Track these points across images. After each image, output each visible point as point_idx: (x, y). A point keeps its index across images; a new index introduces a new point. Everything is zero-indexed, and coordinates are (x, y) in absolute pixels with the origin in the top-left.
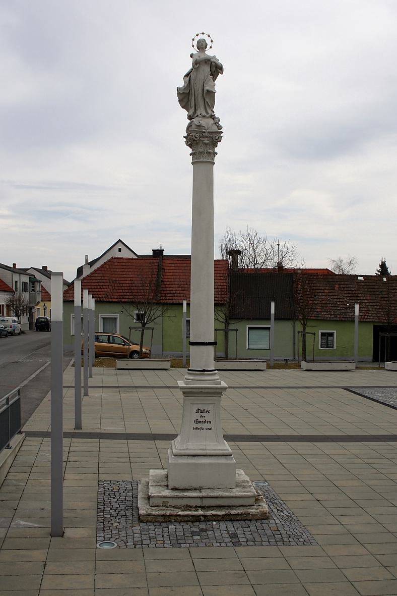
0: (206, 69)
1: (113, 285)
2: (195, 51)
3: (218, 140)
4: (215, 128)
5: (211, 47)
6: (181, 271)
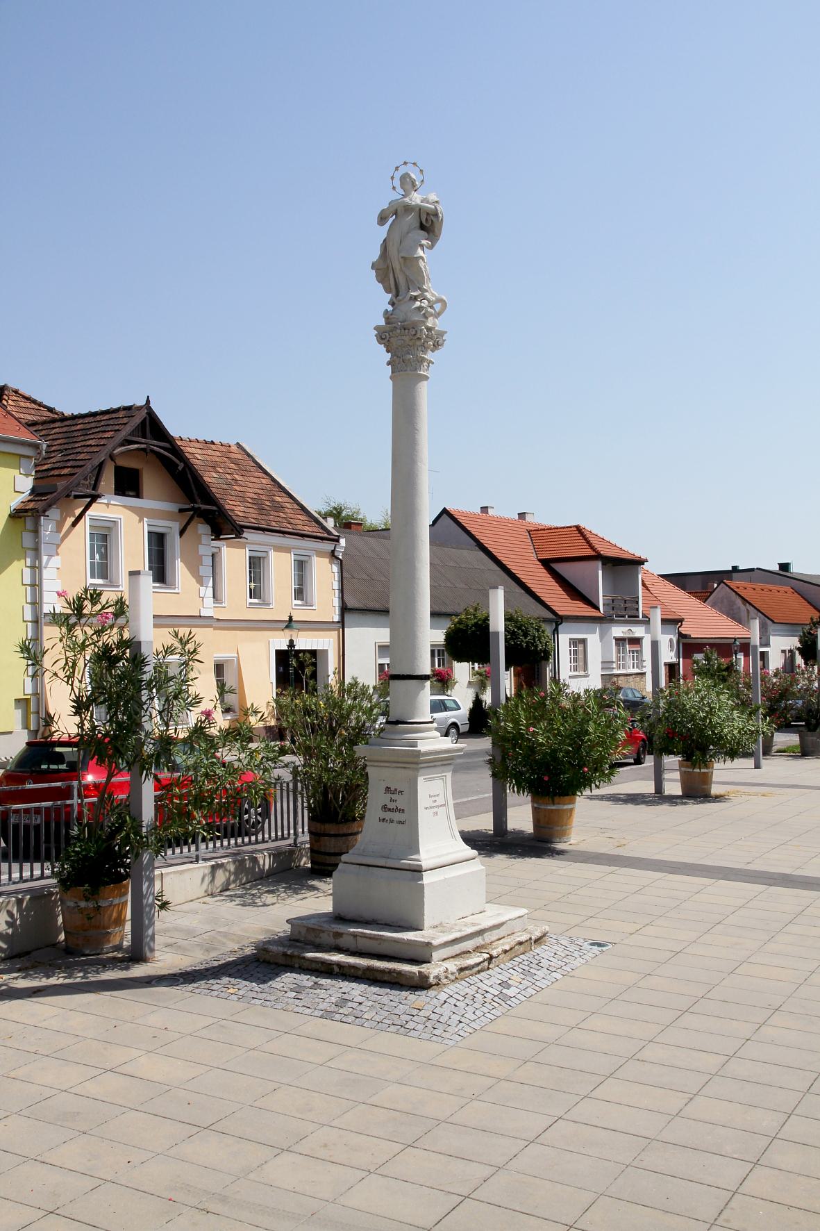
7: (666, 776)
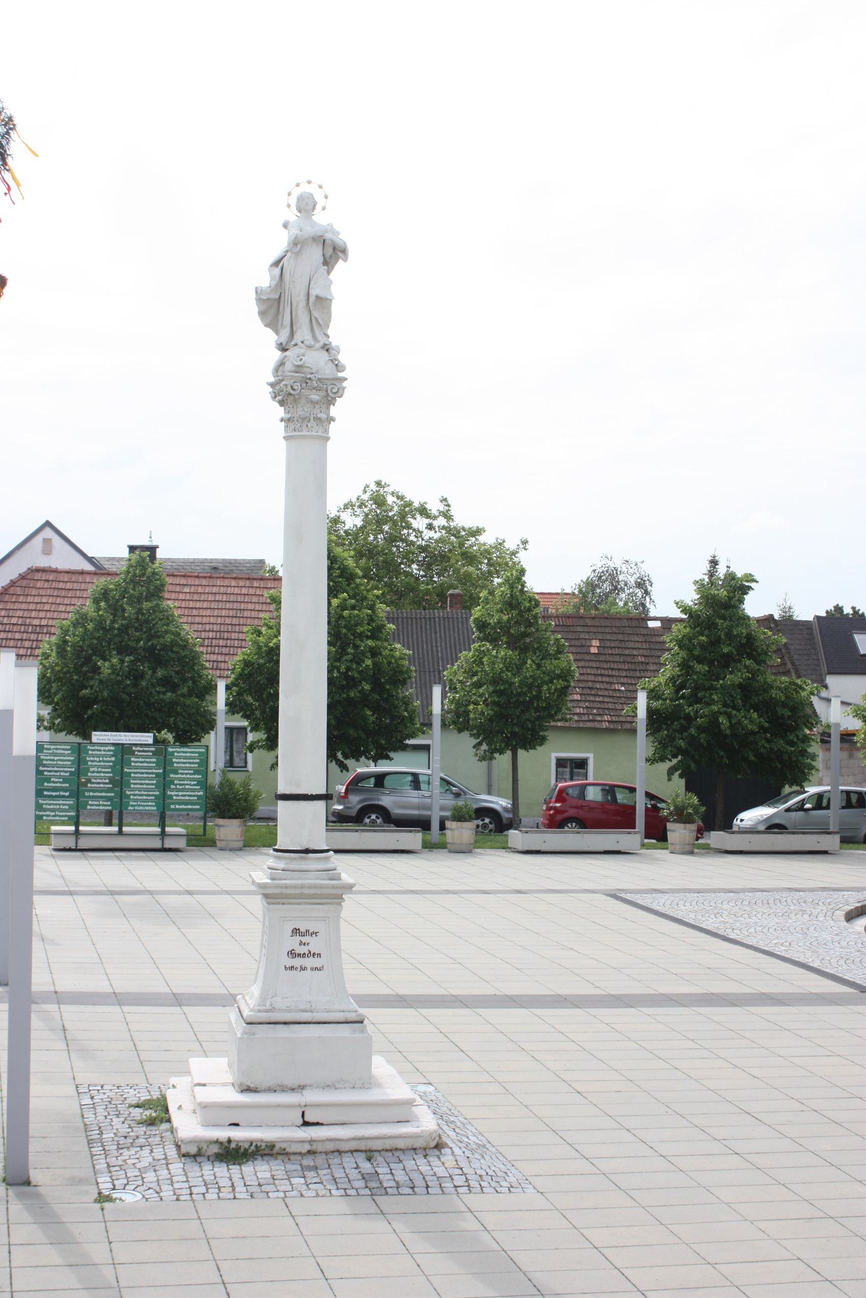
0: (315, 254)
1: (33, 637)
2: (292, 216)
3: (339, 395)
4: (328, 371)
5: (324, 209)
6: (205, 605)
7: (217, 604)
